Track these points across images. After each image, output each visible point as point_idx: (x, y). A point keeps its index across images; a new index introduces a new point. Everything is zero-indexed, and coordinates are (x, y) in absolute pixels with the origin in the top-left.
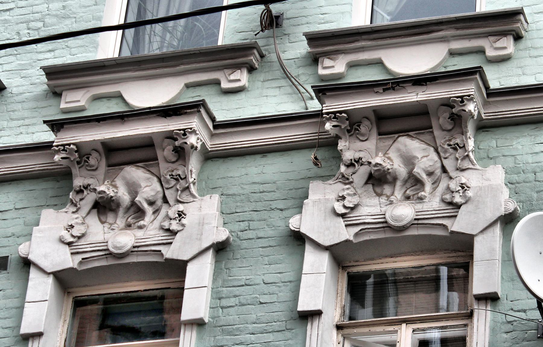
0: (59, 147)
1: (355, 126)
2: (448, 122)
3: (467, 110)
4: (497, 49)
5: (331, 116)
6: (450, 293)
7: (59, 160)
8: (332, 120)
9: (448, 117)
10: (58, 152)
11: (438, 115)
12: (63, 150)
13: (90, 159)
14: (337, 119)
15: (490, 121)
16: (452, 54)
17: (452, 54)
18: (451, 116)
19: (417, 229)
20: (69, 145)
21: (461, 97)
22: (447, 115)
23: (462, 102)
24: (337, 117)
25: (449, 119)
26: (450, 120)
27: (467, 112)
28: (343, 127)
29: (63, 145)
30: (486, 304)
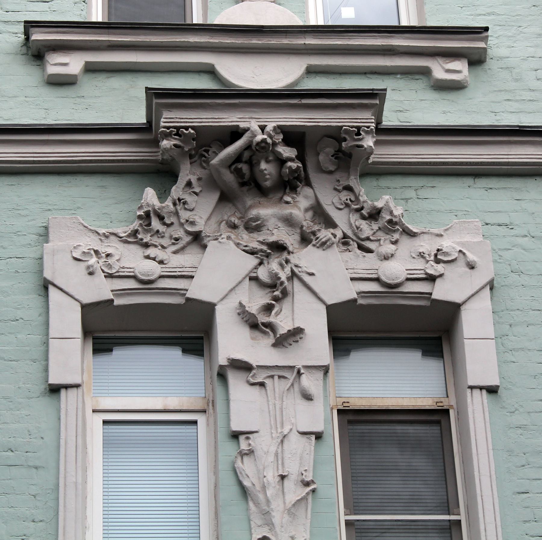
2: (331, 160)
3: (366, 146)
4: (448, 71)
7: (171, 148)
8: (173, 136)
9: (332, 155)
10: (167, 136)
11: (318, 149)
14: (180, 136)
18: (336, 153)
20: (187, 128)
21: (359, 128)
22: (330, 150)
23: (358, 134)
24: (180, 132)
25: (332, 156)
26: (333, 158)
28: (186, 149)
30: (450, 344)
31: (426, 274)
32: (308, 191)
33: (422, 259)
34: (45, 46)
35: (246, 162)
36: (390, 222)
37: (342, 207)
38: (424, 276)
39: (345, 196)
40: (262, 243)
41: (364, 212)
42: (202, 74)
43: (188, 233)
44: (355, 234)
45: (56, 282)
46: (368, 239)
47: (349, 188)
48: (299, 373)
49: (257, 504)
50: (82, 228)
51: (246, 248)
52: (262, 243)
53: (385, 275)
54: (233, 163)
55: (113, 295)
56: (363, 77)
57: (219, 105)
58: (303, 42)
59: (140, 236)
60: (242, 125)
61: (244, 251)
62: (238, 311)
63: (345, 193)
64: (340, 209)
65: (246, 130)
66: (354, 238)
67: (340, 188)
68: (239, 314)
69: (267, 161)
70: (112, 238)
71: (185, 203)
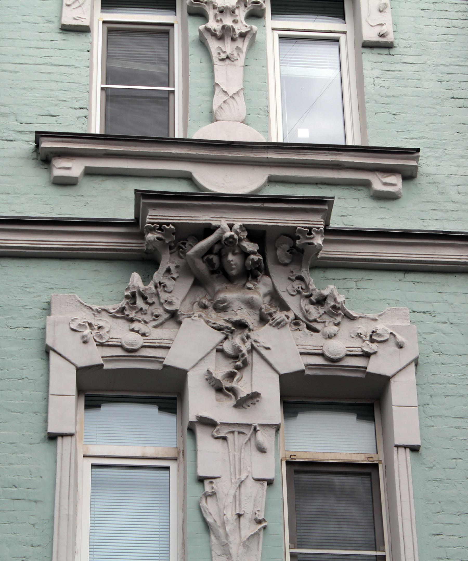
0: (155, 225)
1: (179, 244)
2: (286, 254)
3: (316, 244)
4: (385, 184)
5: (156, 226)
6: (385, 555)
8: (157, 231)
9: (287, 250)
10: (151, 230)
12: (160, 229)
13: (186, 245)
14: (162, 230)
15: (434, 265)
16: (272, 180)
17: (272, 180)
19: (47, 386)
20: (168, 224)
21: (310, 229)
25: (288, 251)
27: (315, 246)
29: (161, 224)
31: (363, 351)
32: (266, 279)
33: (359, 339)
34: (52, 153)
35: (216, 254)
36: (334, 307)
37: (294, 293)
38: (361, 353)
39: (297, 285)
40: (228, 321)
41: (312, 298)
42: (182, 181)
43: (167, 311)
44: (305, 317)
45: (56, 349)
46: (315, 321)
47: (300, 279)
48: (255, 430)
49: (217, 537)
50: (79, 304)
51: (214, 325)
52: (228, 321)
53: (328, 351)
54: (205, 255)
55: (103, 360)
56: (315, 186)
57: (195, 206)
58: (266, 156)
59: (126, 313)
60: (214, 223)
61: (212, 327)
62: (206, 377)
63: (297, 282)
64: (293, 295)
65: (217, 227)
66: (304, 320)
67: (293, 278)
68: (207, 380)
69: (234, 254)
70: (104, 313)
71: (164, 286)
